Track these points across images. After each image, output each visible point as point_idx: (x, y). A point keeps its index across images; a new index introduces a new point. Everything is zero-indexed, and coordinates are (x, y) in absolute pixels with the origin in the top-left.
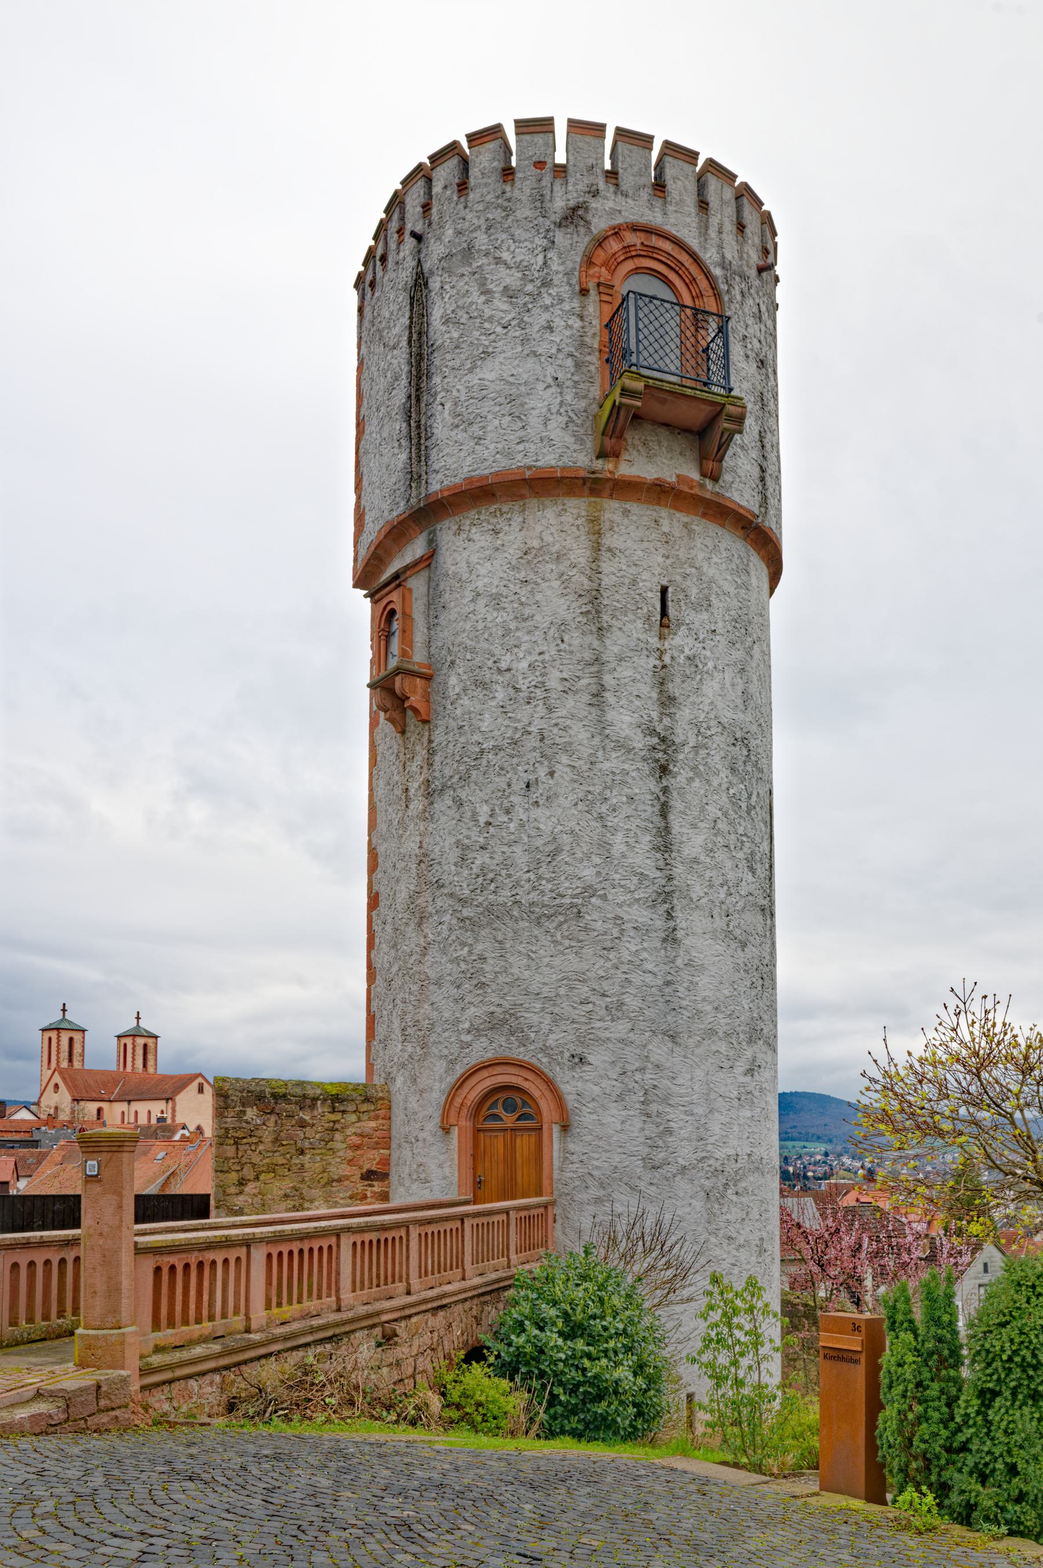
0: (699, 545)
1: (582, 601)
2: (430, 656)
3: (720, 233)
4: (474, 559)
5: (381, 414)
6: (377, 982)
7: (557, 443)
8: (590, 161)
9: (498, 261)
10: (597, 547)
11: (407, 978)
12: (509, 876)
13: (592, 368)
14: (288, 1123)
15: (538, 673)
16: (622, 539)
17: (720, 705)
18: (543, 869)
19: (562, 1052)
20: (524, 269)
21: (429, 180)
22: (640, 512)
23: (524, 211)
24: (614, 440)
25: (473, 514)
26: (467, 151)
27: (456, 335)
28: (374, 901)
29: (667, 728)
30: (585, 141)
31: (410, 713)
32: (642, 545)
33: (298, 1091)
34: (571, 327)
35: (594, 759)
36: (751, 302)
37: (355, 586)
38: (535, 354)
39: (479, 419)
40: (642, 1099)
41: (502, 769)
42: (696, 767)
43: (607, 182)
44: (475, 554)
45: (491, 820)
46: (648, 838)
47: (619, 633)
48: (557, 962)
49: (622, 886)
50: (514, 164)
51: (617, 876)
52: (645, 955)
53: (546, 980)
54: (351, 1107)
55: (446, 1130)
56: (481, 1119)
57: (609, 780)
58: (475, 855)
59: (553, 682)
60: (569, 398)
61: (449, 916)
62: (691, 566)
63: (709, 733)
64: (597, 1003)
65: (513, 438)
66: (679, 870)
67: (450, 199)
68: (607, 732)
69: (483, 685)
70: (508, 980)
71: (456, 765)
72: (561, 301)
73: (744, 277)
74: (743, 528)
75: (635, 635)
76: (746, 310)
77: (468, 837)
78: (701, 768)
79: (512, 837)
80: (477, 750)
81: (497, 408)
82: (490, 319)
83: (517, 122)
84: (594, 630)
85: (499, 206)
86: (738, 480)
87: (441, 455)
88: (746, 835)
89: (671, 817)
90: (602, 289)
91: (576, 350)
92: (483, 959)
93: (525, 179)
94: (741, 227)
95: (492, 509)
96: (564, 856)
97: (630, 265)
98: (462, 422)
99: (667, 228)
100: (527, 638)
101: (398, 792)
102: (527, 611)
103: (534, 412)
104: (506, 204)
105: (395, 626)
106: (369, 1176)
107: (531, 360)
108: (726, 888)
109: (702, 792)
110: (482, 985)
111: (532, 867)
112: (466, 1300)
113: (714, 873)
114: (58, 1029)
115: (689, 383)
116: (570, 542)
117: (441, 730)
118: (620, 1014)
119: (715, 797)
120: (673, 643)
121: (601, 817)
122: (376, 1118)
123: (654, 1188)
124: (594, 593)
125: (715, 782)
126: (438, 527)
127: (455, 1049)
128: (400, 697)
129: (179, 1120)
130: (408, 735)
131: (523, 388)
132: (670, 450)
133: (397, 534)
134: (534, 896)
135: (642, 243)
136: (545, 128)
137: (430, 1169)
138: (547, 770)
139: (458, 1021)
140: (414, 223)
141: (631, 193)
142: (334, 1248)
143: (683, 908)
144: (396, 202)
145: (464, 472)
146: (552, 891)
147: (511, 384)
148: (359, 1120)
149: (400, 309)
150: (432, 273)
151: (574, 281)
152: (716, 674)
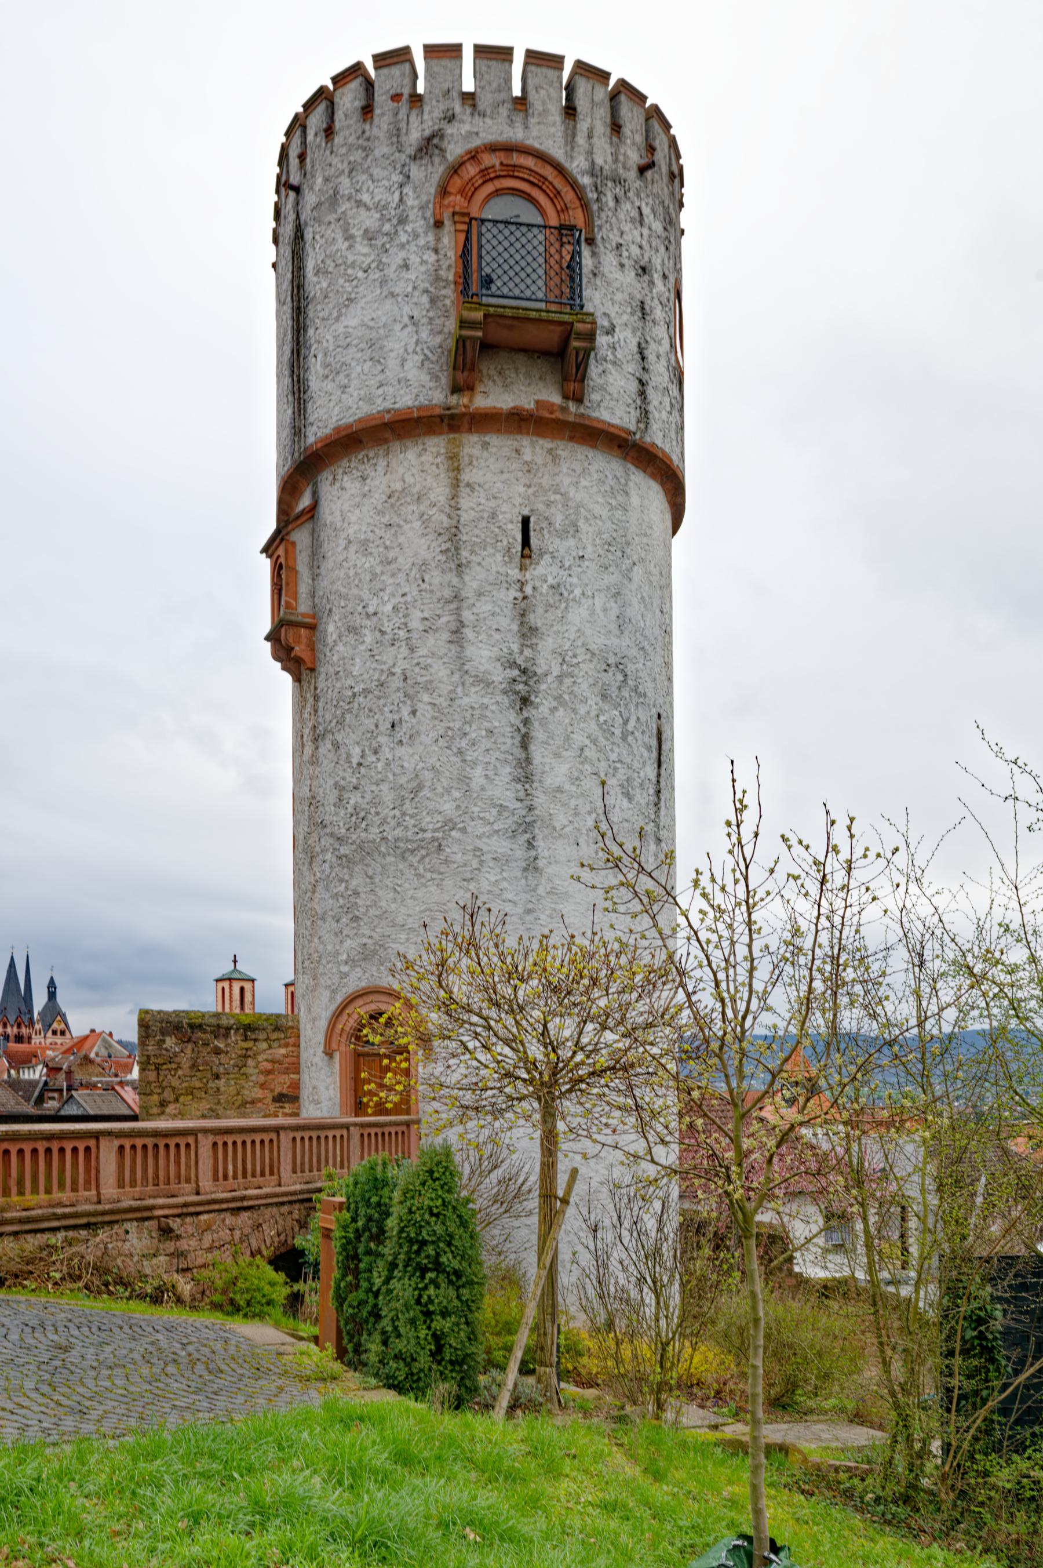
0: (565, 470)
1: (441, 539)
3: (590, 137)
4: (346, 507)
7: (411, 379)
8: (445, 86)
9: (359, 203)
10: (456, 484)
12: (377, 813)
13: (448, 302)
14: (205, 1051)
16: (481, 473)
17: (588, 632)
18: (407, 805)
20: (381, 207)
22: (500, 444)
23: (382, 149)
24: (466, 374)
25: (345, 463)
27: (324, 285)
30: (439, 65)
32: (502, 475)
33: (214, 1021)
34: (426, 262)
35: (453, 696)
36: (628, 206)
38: (392, 295)
42: (561, 696)
43: (463, 104)
46: (508, 770)
47: (478, 568)
48: (420, 894)
50: (421, 89)
51: (476, 809)
52: (505, 884)
53: (410, 912)
54: (262, 1036)
55: (329, 1054)
57: (468, 715)
58: (349, 795)
59: (415, 624)
60: (424, 335)
62: (555, 493)
63: (575, 661)
65: (373, 383)
66: (541, 800)
67: (319, 146)
68: (466, 667)
69: (353, 630)
70: (378, 913)
72: (416, 236)
73: (618, 181)
74: (619, 447)
75: (494, 569)
76: (622, 216)
77: (344, 779)
78: (566, 697)
81: (360, 355)
82: (353, 265)
84: (453, 566)
85: (360, 147)
86: (608, 397)
89: (532, 748)
90: (457, 218)
92: (356, 893)
93: (383, 114)
95: (360, 457)
96: (426, 792)
97: (489, 188)
98: (333, 371)
99: (530, 142)
100: (391, 581)
102: (391, 555)
103: (392, 355)
104: (365, 144)
106: (280, 1099)
107: (389, 301)
108: (594, 815)
109: (567, 721)
110: (356, 919)
111: (397, 804)
112: (283, 1204)
113: (580, 801)
114: (230, 980)
116: (430, 481)
117: (322, 677)
120: (536, 573)
121: (460, 752)
122: (287, 1045)
124: (453, 530)
125: (582, 710)
127: (336, 979)
131: (382, 331)
132: (528, 375)
134: (398, 832)
135: (501, 164)
136: (402, 58)
138: (409, 709)
139: (337, 953)
141: (488, 112)
142: (94, 1150)
143: (545, 838)
145: (332, 424)
146: (414, 826)
147: (371, 328)
148: (270, 1047)
151: (429, 214)
152: (583, 601)
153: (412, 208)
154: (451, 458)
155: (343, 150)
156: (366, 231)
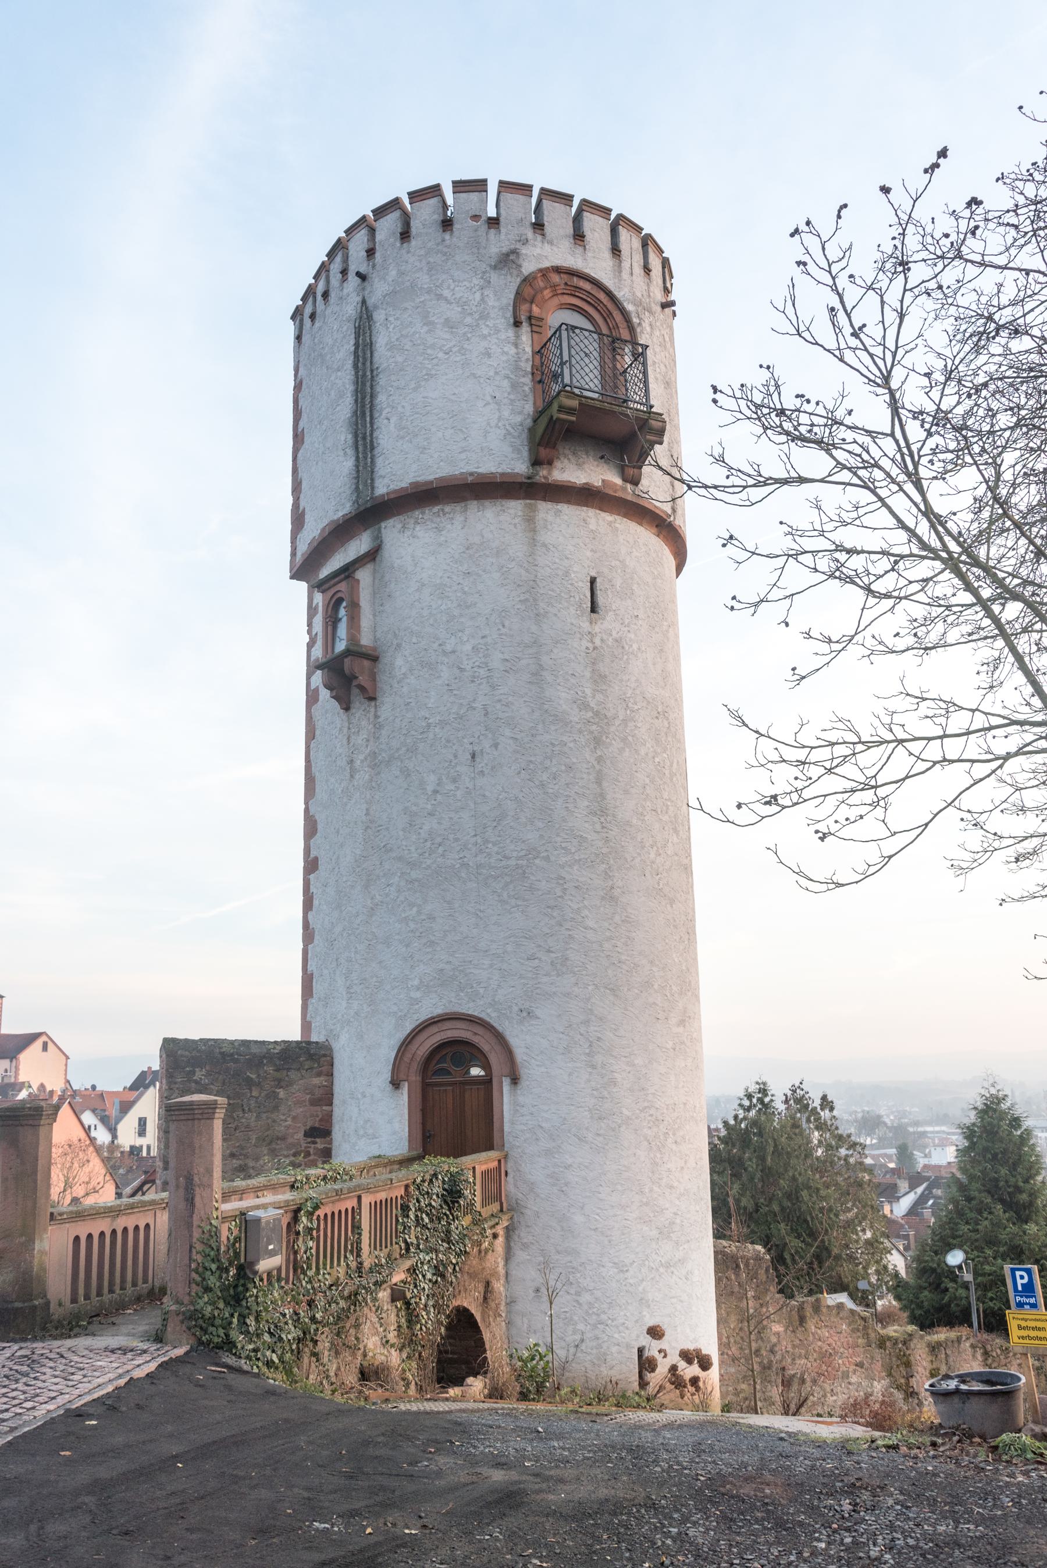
2: (376, 640)
5: (324, 427)
6: (316, 941)
9: (440, 297)
10: (533, 542)
11: (352, 937)
12: (457, 840)
13: (526, 388)
15: (481, 655)
19: (510, 1007)
21: (372, 231)
25: (417, 513)
26: (409, 206)
27: (400, 359)
28: (311, 865)
29: (600, 703)
31: (355, 691)
34: (507, 353)
35: (534, 732)
37: (292, 578)
39: (423, 432)
40: (587, 1051)
41: (448, 741)
44: (414, 546)
45: (438, 788)
49: (563, 848)
51: (559, 839)
55: (395, 1084)
56: (430, 1073)
59: (496, 663)
60: (506, 413)
61: (397, 878)
63: (636, 707)
64: (543, 958)
71: (402, 738)
74: (657, 526)
76: (655, 340)
78: (630, 738)
79: (459, 804)
80: (424, 724)
82: (433, 346)
83: (454, 182)
87: (387, 462)
88: (670, 800)
89: (605, 784)
91: (512, 372)
92: (432, 918)
94: (647, 270)
99: (587, 271)
101: (342, 762)
105: (342, 612)
108: (655, 848)
109: (632, 760)
110: (432, 943)
115: (609, 400)
118: (564, 970)
119: (643, 765)
121: (542, 785)
122: (319, 1075)
123: (601, 1139)
124: (531, 583)
125: (643, 752)
126: (383, 525)
128: (346, 675)
129: (22, 1078)
130: (353, 711)
133: (340, 532)
134: (481, 859)
137: (374, 1121)
144: (339, 247)
146: (497, 853)
149: (344, 337)
150: (376, 307)
152: (639, 655)
153: (494, 307)
154: (529, 520)
155: (422, 252)
156: (447, 320)
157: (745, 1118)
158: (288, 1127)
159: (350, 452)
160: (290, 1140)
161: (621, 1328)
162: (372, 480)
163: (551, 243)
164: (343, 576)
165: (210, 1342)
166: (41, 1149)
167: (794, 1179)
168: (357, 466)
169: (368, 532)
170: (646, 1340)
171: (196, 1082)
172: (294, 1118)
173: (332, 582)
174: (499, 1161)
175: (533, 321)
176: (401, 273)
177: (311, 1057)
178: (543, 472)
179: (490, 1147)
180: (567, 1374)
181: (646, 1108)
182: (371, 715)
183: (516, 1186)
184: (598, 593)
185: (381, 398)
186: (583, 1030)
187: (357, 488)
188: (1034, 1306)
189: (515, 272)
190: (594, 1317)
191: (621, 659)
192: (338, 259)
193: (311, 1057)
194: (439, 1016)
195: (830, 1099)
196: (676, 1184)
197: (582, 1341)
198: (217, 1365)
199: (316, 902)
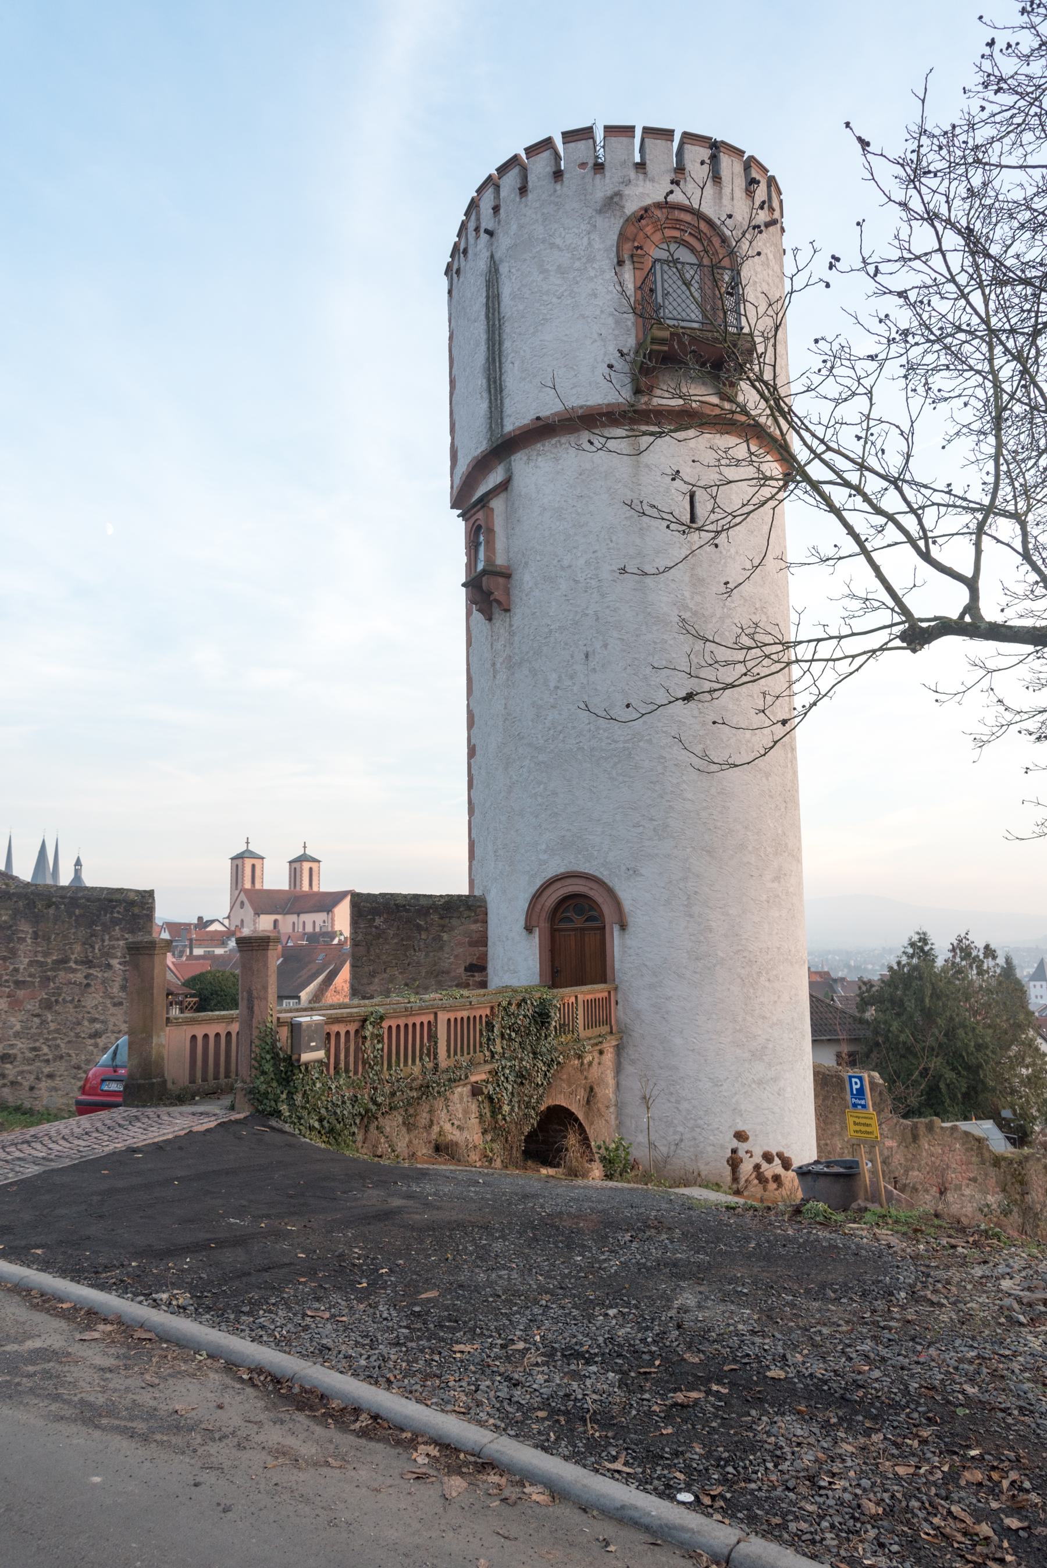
9: (553, 245)
12: (574, 728)
13: (629, 323)
19: (619, 866)
21: (497, 187)
27: (521, 307)
31: (495, 604)
38: (583, 316)
44: (537, 473)
51: (660, 724)
55: (529, 929)
92: (555, 793)
101: (488, 665)
104: (557, 200)
105: (482, 538)
121: (646, 678)
122: (476, 922)
126: (513, 458)
128: (488, 592)
130: (494, 621)
133: (482, 466)
137: (516, 959)
140: (487, 223)
144: (473, 206)
146: (608, 738)
150: (501, 261)
152: (737, 558)
153: (599, 250)
155: (538, 205)
157: (908, 964)
158: (451, 964)
159: (485, 395)
160: (453, 974)
161: (716, 1132)
162: (502, 419)
163: (653, 180)
164: (479, 506)
165: (264, 1110)
166: (156, 971)
167: (951, 1019)
168: (490, 408)
169: (502, 465)
170: (735, 1143)
171: (376, 927)
172: (456, 956)
173: (472, 512)
174: (609, 992)
175: (635, 259)
176: (521, 227)
177: (469, 908)
178: (644, 399)
179: (604, 981)
180: (668, 1167)
181: (739, 951)
182: (507, 624)
183: (625, 1013)
184: (697, 505)
185: (507, 344)
186: (682, 885)
187: (491, 427)
188: (864, 1106)
189: (618, 213)
190: (692, 1122)
191: (719, 563)
192: (473, 217)
193: (469, 908)
194: (562, 874)
195: (993, 946)
196: (768, 1015)
197: (682, 1140)
198: (264, 1126)
199: (475, 782)
